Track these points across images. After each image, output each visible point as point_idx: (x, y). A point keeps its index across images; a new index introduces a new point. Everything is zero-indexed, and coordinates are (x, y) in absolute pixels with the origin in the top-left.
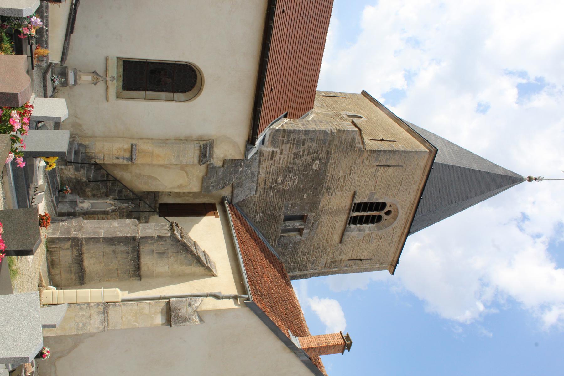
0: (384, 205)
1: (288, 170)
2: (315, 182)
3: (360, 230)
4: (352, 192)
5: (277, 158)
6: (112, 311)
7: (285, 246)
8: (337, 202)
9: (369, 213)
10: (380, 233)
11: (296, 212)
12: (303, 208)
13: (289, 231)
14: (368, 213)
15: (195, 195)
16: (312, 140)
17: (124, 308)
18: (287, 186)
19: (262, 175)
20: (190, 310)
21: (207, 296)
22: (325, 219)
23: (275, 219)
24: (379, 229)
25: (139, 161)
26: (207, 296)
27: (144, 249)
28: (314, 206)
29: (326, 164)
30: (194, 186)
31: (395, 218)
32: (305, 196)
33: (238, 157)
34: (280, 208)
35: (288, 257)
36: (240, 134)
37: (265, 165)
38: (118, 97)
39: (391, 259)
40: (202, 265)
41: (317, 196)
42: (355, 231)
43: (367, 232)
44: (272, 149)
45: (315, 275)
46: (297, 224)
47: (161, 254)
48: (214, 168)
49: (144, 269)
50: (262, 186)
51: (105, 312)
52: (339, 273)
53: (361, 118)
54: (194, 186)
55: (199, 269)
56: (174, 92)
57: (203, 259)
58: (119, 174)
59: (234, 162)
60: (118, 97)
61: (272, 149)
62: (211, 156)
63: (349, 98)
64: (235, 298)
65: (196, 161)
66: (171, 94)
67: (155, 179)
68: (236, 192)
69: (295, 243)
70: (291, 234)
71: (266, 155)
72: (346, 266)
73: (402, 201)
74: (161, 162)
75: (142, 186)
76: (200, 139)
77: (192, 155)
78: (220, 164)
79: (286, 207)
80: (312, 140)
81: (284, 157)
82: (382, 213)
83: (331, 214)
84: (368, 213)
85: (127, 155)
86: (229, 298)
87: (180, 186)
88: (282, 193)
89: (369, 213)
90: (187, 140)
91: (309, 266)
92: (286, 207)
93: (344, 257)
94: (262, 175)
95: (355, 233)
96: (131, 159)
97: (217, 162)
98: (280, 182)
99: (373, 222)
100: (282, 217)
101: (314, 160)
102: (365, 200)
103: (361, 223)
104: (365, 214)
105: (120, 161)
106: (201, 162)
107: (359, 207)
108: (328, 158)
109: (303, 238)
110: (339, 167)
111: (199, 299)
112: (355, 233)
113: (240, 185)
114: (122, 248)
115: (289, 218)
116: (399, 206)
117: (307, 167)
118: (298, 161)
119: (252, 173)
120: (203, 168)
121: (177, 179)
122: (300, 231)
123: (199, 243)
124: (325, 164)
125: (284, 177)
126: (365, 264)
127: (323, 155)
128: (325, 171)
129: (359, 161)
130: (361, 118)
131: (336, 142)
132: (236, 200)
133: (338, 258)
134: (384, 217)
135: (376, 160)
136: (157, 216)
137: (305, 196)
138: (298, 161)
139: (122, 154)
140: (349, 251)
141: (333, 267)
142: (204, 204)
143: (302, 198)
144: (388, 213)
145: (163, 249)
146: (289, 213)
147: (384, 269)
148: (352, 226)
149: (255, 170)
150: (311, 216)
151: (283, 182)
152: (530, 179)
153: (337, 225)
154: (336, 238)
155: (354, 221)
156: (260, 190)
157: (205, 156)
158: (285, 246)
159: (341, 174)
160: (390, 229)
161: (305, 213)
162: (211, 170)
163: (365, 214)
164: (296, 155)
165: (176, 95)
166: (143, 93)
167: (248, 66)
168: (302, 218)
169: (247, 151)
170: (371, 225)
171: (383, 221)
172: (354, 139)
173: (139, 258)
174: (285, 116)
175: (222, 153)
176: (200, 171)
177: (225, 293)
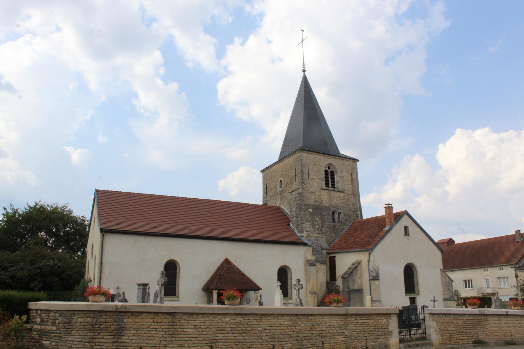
0: (326, 171)
1: (313, 224)
2: (318, 209)
3: (338, 183)
4: (321, 190)
5: (308, 229)
6: (374, 299)
7: (346, 220)
8: (326, 198)
9: (330, 178)
10: (339, 171)
11: (330, 217)
12: (329, 214)
13: (339, 219)
14: (329, 178)
15: (326, 266)
16: (300, 214)
17: (373, 295)
18: (320, 223)
19: (316, 235)
20: (374, 272)
21: (369, 264)
22: (333, 202)
23: (334, 227)
24: (337, 172)
25: (315, 290)
26: (369, 264)
27: (352, 288)
28: (328, 209)
29: (309, 205)
30: (324, 267)
31: (331, 164)
32: (324, 214)
33: (311, 249)
34: (330, 225)
35: (352, 218)
36: (302, 249)
37: (311, 234)
38: (291, 299)
39: (352, 162)
40: (357, 265)
41: (323, 208)
42: (338, 185)
43: (339, 179)
44: (305, 232)
45: (359, 203)
46: (336, 216)
47: (354, 281)
48: (316, 259)
49: (359, 288)
50: (320, 235)
51: (374, 301)
52: (358, 190)
53: (281, 181)
54: (324, 267)
55: (359, 267)
56: (287, 277)
57: (355, 265)
58: (320, 298)
59: (313, 250)
60: (291, 299)
61: (305, 232)
62: (312, 260)
63: (266, 181)
64: (370, 254)
65: (314, 267)
66: (288, 278)
67: (321, 283)
68: (324, 248)
69: (345, 215)
70: (340, 218)
71: (307, 234)
72: (355, 187)
73: (323, 161)
74: (315, 281)
75: (324, 288)
76: (305, 265)
77: (313, 269)
78: (314, 256)
79: (329, 222)
80: (300, 214)
81: (307, 226)
82: (329, 171)
83: (331, 200)
84: (329, 178)
85: (314, 295)
86: (369, 256)
87: (324, 273)
88: (323, 225)
89: (330, 178)
90: (306, 271)
91: (355, 207)
92: (329, 222)
93: (351, 189)
94: (316, 235)
95: (339, 185)
96: (315, 293)
97: (314, 258)
98: (309, 210)
99: (334, 175)
100: (333, 223)
101: (308, 212)
102: (324, 182)
103: (334, 182)
104: (330, 180)
105: (316, 297)
106: (315, 265)
107: (327, 185)
108: (307, 205)
109: (342, 212)
110: (310, 199)
111: (370, 268)
112: (339, 185)
113: (321, 246)
114: (352, 296)
115: (334, 221)
116: (326, 164)
117: (311, 215)
118: (309, 219)
119: (315, 240)
120: (317, 264)
121: (321, 274)
122: (339, 213)
123: (349, 267)
124: (309, 206)
125: (316, 225)
126: (354, 177)
127: (306, 207)
128: (313, 206)
129: (307, 189)
130: (281, 181)
131: (300, 202)
132: (327, 247)
133: (351, 192)
134: (331, 170)
135: (306, 180)
136: (336, 282)
137: (324, 214)
138: (309, 219)
139: (313, 297)
140: (348, 187)
141: (356, 194)
142: (330, 261)
143: (325, 215)
144: (329, 168)
145: (352, 281)
146: (332, 221)
147: (356, 165)
148: (336, 186)
149: (314, 239)
150: (332, 209)
151: (318, 225)
152: (304, 71)
153: (336, 195)
154: (342, 194)
155: (333, 185)
156: (322, 235)
157: (312, 263)
158: (346, 220)
159: (313, 197)
160: (337, 167)
161: (331, 213)
162: (317, 261)
163: (330, 180)
164: (307, 220)
165: (289, 276)
166: (289, 289)
167: (277, 248)
168: (333, 213)
169: (309, 246)
170: (335, 176)
171: (333, 170)
172: (298, 193)
173: (355, 290)
174: (289, 225)
175: (310, 257)
176: (318, 264)
177: (367, 258)
